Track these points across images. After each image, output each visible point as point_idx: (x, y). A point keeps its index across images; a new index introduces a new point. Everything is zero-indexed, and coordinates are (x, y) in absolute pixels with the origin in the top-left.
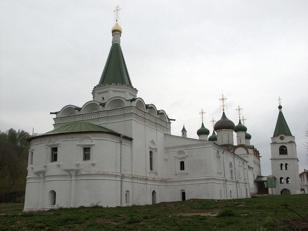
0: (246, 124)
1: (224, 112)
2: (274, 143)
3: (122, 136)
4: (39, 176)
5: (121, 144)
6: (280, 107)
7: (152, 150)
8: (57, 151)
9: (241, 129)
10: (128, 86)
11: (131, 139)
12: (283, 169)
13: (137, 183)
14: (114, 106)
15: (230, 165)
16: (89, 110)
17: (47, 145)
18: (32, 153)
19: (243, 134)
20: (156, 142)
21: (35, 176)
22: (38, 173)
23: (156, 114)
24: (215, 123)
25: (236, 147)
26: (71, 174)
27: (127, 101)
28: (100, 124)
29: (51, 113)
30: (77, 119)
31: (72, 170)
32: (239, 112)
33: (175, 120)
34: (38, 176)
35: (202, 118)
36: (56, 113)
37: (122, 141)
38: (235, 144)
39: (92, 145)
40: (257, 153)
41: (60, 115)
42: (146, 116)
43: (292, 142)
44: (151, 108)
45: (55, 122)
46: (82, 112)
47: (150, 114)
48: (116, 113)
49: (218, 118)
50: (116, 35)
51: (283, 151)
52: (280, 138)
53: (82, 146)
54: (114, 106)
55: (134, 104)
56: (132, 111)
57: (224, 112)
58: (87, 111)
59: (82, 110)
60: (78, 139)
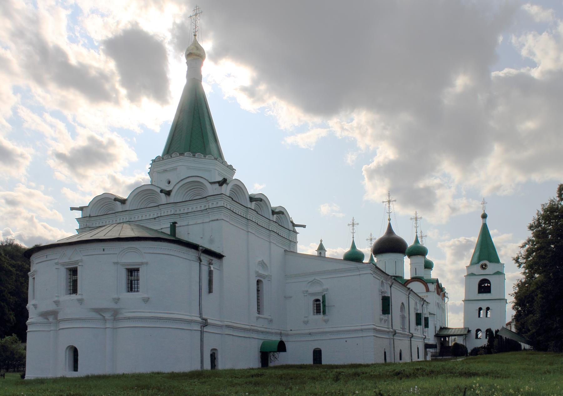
0: (425, 243)
1: (353, 241)
2: (471, 275)
4: (47, 319)
6: (484, 216)
9: (418, 252)
10: (216, 159)
11: (219, 256)
12: (481, 316)
15: (401, 308)
17: (57, 264)
18: (34, 278)
19: (419, 260)
20: (268, 265)
21: (41, 319)
22: (45, 315)
24: (374, 242)
25: (408, 282)
29: (72, 209)
32: (416, 223)
33: (304, 226)
34: (45, 320)
35: (353, 233)
36: (81, 209)
37: (202, 258)
38: (407, 276)
39: (142, 264)
40: (440, 290)
43: (499, 273)
44: (259, 200)
45: (80, 226)
46: (127, 207)
49: (380, 233)
51: (484, 287)
52: (482, 266)
53: (123, 265)
55: (226, 190)
56: (221, 204)
57: (353, 241)
59: (128, 203)
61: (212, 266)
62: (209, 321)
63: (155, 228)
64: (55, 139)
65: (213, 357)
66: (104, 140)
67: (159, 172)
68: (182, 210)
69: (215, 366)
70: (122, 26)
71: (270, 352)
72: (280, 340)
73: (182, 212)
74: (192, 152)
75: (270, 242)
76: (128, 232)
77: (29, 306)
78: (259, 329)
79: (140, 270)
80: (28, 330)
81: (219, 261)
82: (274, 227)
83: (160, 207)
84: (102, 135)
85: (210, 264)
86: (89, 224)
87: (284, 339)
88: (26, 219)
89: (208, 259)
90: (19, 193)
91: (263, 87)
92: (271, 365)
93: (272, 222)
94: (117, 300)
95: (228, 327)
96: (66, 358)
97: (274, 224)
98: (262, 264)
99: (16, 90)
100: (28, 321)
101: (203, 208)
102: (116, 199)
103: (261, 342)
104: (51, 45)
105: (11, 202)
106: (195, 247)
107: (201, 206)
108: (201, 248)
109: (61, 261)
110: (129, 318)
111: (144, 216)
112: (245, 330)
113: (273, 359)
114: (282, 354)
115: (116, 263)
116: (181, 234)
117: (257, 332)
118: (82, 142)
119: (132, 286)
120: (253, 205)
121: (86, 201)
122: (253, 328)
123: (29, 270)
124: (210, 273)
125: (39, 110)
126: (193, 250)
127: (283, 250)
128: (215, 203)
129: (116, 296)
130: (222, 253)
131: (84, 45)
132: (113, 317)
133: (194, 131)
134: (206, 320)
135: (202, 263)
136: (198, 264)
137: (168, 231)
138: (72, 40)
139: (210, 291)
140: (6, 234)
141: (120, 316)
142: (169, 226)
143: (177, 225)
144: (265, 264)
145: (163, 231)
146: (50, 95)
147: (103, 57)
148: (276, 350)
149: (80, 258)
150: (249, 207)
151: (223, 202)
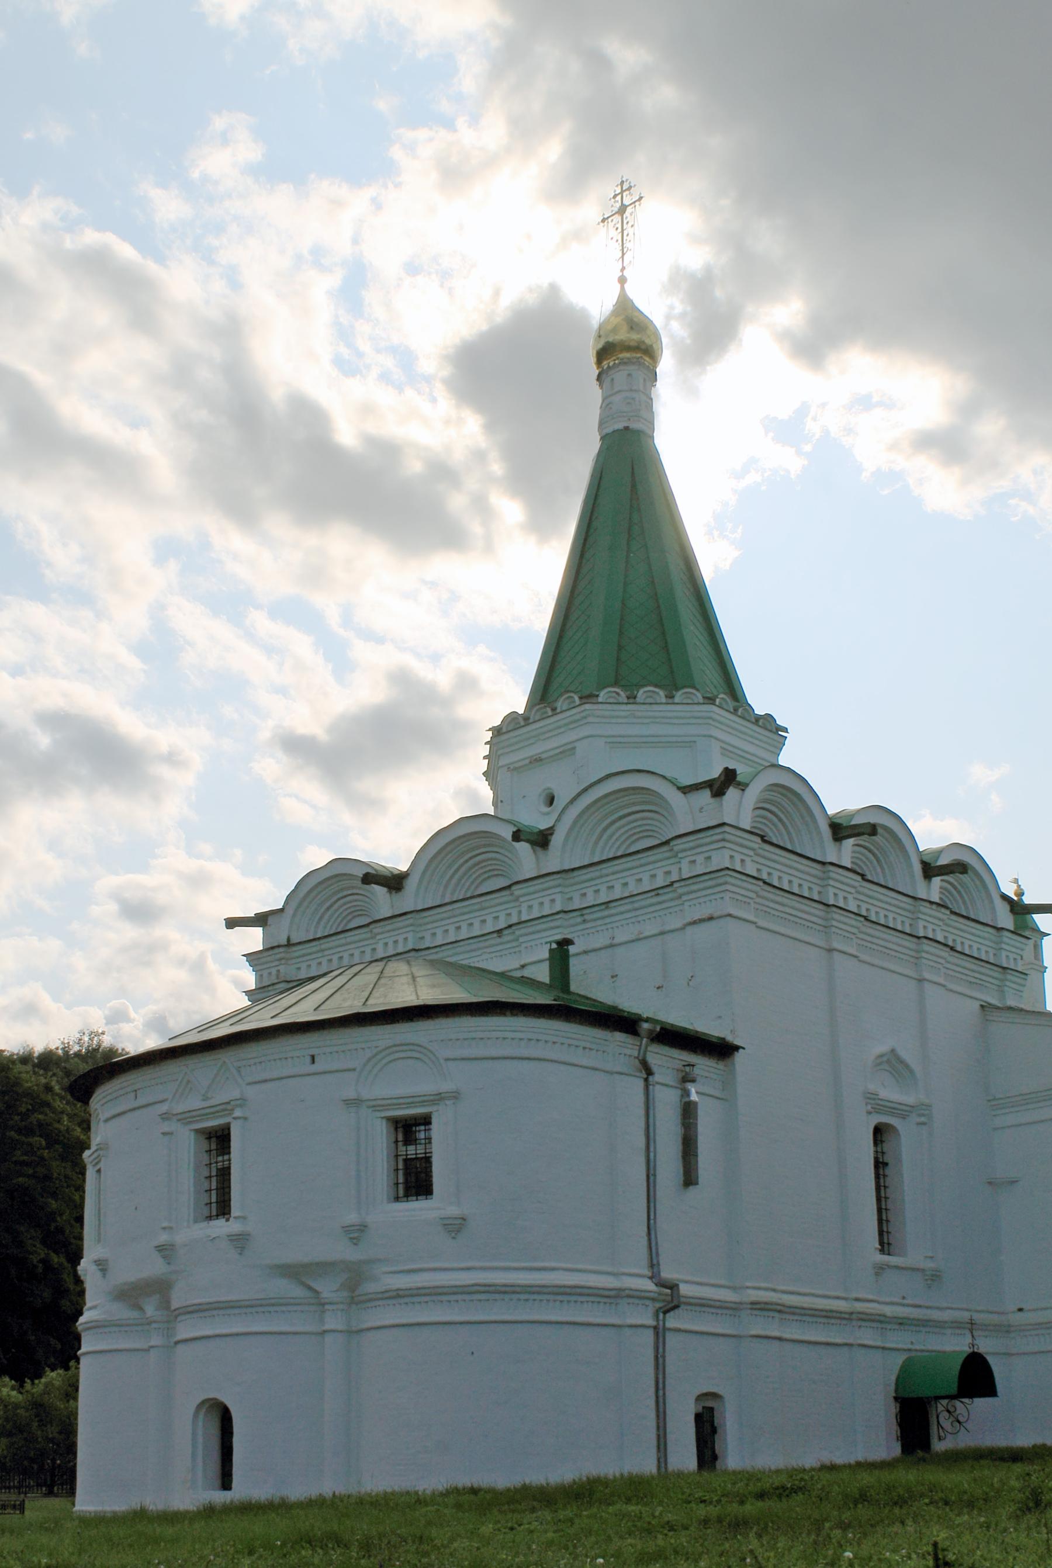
3: (651, 1031)
4: (141, 1309)
5: (646, 1080)
7: (893, 1114)
8: (229, 1153)
10: (710, 700)
11: (722, 1050)
13: (780, 1339)
14: (611, 837)
16: (454, 881)
17: (165, 1117)
18: (99, 1171)
21: (122, 1312)
22: (130, 1294)
23: (912, 876)
26: (317, 1292)
27: (689, 795)
28: (523, 966)
29: (232, 923)
30: (386, 944)
31: (323, 1268)
34: (135, 1314)
36: (261, 920)
39: (439, 1098)
41: (281, 932)
42: (831, 891)
44: (871, 832)
45: (259, 978)
46: (408, 900)
47: (863, 876)
48: (626, 884)
50: (620, 377)
53: (376, 1106)
54: (613, 834)
55: (739, 808)
56: (721, 859)
58: (442, 889)
59: (411, 885)
60: (350, 1066)
61: (693, 1089)
62: (684, 1289)
63: (498, 965)
64: (282, 691)
65: (706, 1426)
66: (442, 679)
67: (515, 769)
68: (590, 892)
69: (715, 1457)
70: (508, 300)
71: (938, 1398)
72: (967, 1350)
73: (590, 900)
74: (624, 687)
75: (921, 980)
76: (405, 990)
77: (86, 1267)
78: (888, 1310)
79: (434, 1120)
80: (84, 1349)
81: (721, 1065)
82: (931, 923)
83: (517, 890)
84: (435, 658)
85: (686, 1079)
86: (289, 971)
87: (985, 1346)
88: (181, 962)
89: (678, 1065)
90: (154, 881)
91: (990, 428)
92: (939, 1446)
93: (925, 908)
94: (357, 1233)
95: (760, 1307)
96: (194, 1446)
97: (933, 911)
98: (893, 1064)
99: (165, 550)
100: (82, 1320)
101: (660, 882)
102: (373, 877)
103: (900, 1359)
104: (277, 395)
105: (139, 911)
106: (625, 1023)
107: (656, 871)
108: (646, 1026)
109: (180, 1108)
110: (398, 1295)
111: (464, 926)
112: (828, 1316)
113: (946, 1424)
114: (980, 1403)
115: (354, 1103)
116: (591, 982)
117: (879, 1321)
118: (366, 692)
119: (416, 1180)
120: (847, 852)
121: (271, 896)
122: (859, 1306)
123: (85, 1146)
124: (688, 1111)
125: (232, 604)
126: (619, 1036)
127: (976, 1005)
128: (700, 859)
129: (352, 1218)
130: (730, 1038)
131: (385, 377)
132: (345, 1294)
133: (634, 618)
134: (673, 1287)
135: (657, 1078)
136: (641, 1083)
137: (542, 974)
138: (348, 367)
139: (689, 1179)
140: (117, 1017)
141: (370, 1287)
142: (547, 955)
143: (572, 949)
144: (902, 1062)
145: (527, 973)
146: (265, 555)
147: (445, 404)
148: (954, 1389)
149: (236, 1094)
150: (831, 858)
151: (727, 853)
